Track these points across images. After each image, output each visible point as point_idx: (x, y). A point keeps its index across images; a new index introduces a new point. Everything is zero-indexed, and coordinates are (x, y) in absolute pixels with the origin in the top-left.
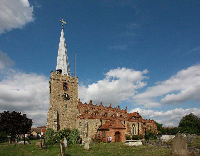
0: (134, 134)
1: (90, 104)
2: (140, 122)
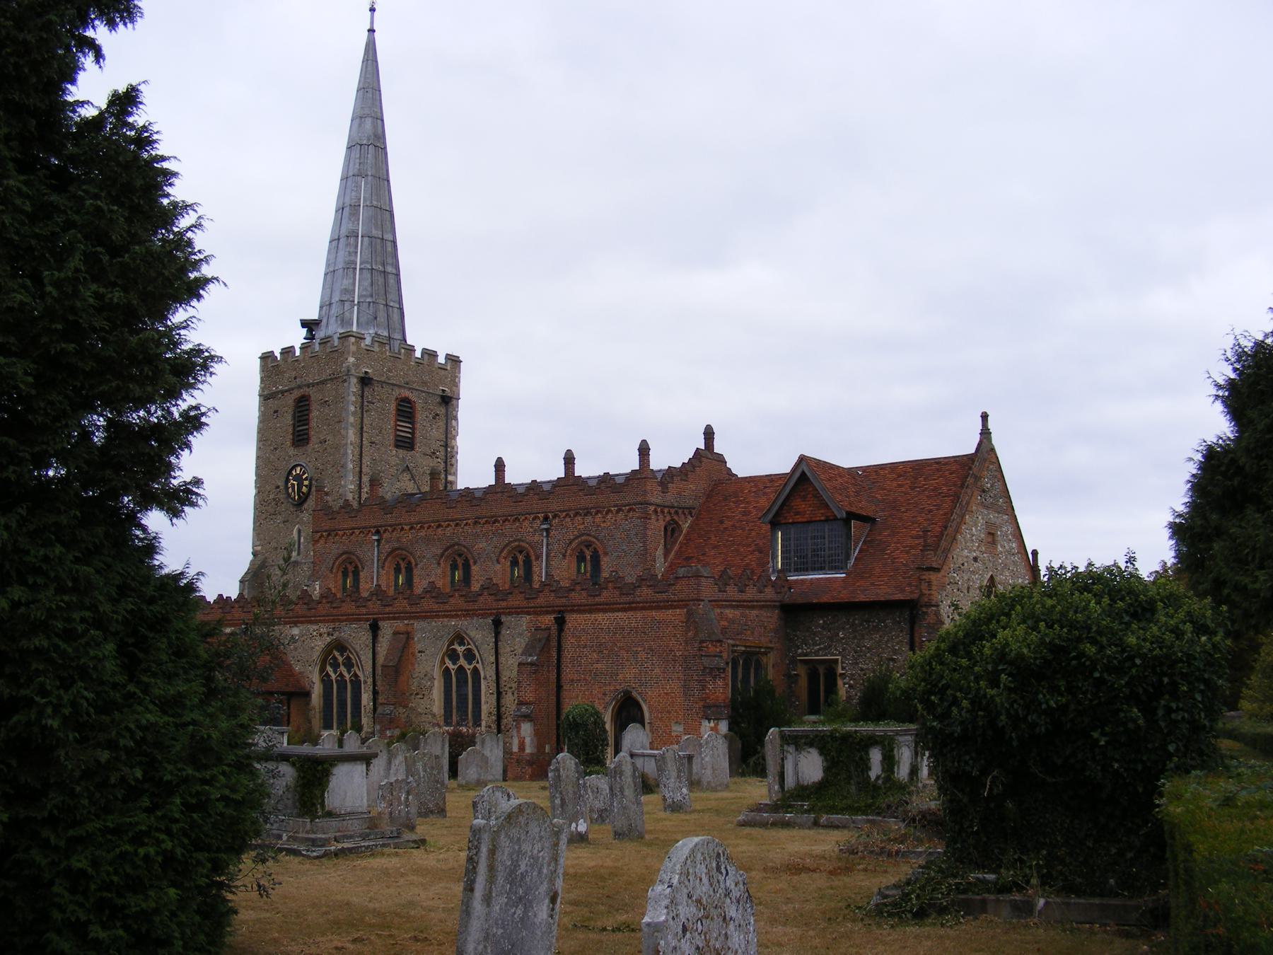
2: (518, 611)
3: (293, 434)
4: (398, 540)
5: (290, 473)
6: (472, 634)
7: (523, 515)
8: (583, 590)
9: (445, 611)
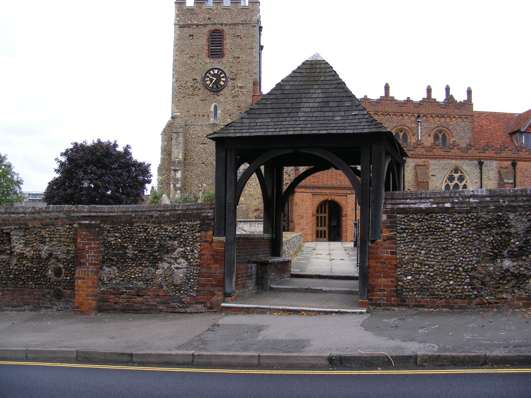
0: (321, 217)
1: (424, 100)
2: (491, 159)
6: (465, 168)
7: (405, 113)
8: (526, 151)
9: (448, 156)
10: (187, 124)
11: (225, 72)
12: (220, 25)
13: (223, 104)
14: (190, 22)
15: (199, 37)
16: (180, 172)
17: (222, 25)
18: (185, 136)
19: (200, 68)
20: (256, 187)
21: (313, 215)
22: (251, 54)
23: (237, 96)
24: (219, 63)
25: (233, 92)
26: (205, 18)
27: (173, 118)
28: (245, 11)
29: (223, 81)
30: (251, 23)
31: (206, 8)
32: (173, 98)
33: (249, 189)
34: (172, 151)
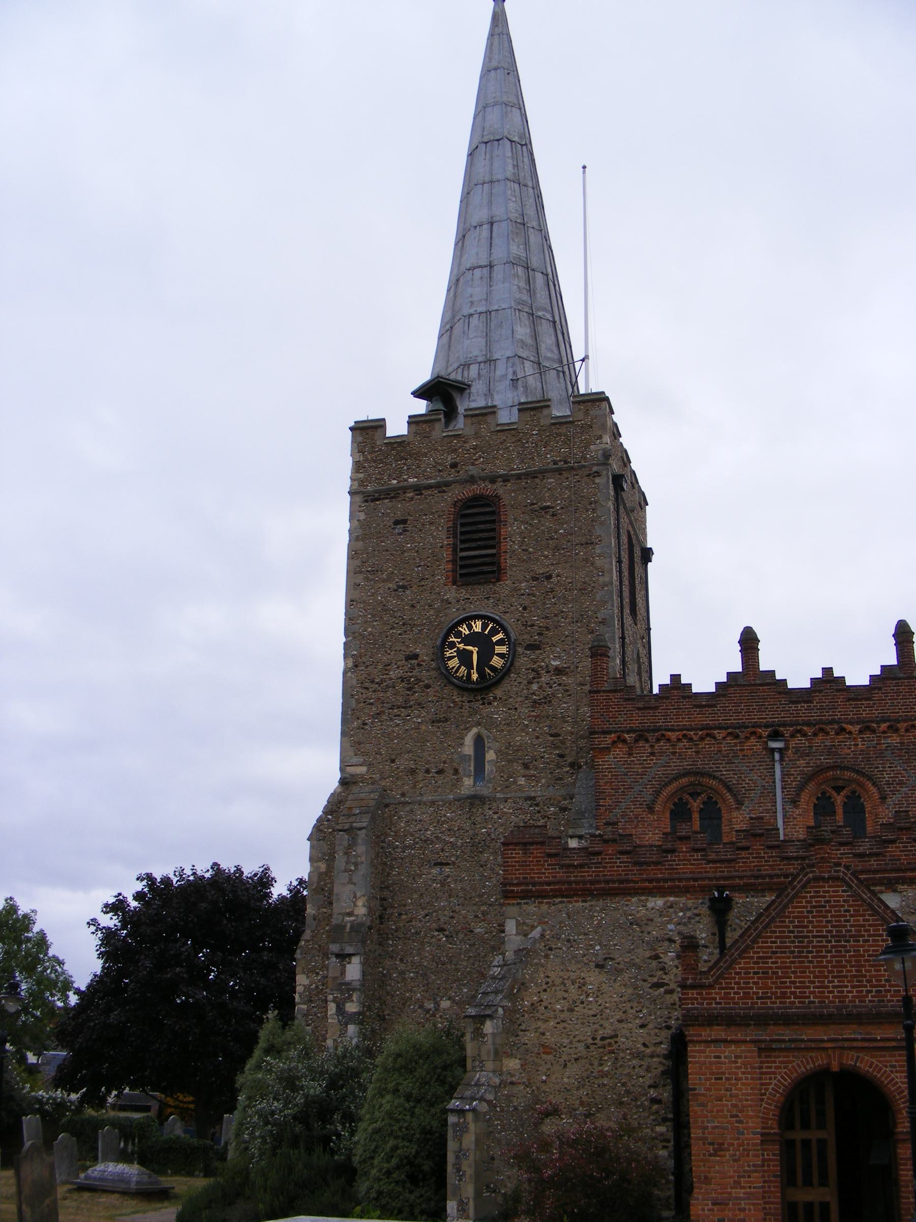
3: (454, 561)
4: (830, 751)
5: (453, 629)
10: (387, 801)
11: (505, 623)
12: (487, 483)
13: (503, 731)
14: (395, 482)
15: (423, 525)
16: (356, 960)
17: (493, 480)
18: (383, 842)
19: (428, 618)
20: (566, 1015)
21: (766, 1139)
22: (586, 560)
23: (547, 700)
24: (488, 598)
25: (535, 687)
26: (440, 464)
27: (344, 782)
28: (563, 430)
29: (501, 655)
30: (584, 466)
31: (444, 435)
32: (344, 721)
33: (540, 1023)
34: (335, 890)
